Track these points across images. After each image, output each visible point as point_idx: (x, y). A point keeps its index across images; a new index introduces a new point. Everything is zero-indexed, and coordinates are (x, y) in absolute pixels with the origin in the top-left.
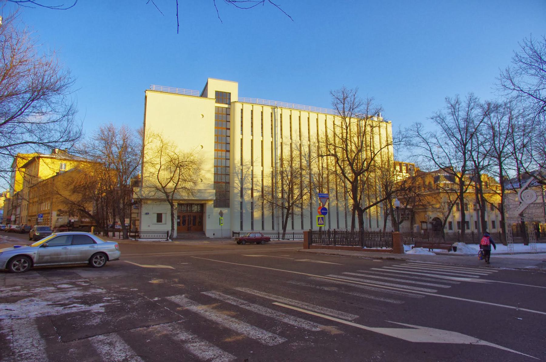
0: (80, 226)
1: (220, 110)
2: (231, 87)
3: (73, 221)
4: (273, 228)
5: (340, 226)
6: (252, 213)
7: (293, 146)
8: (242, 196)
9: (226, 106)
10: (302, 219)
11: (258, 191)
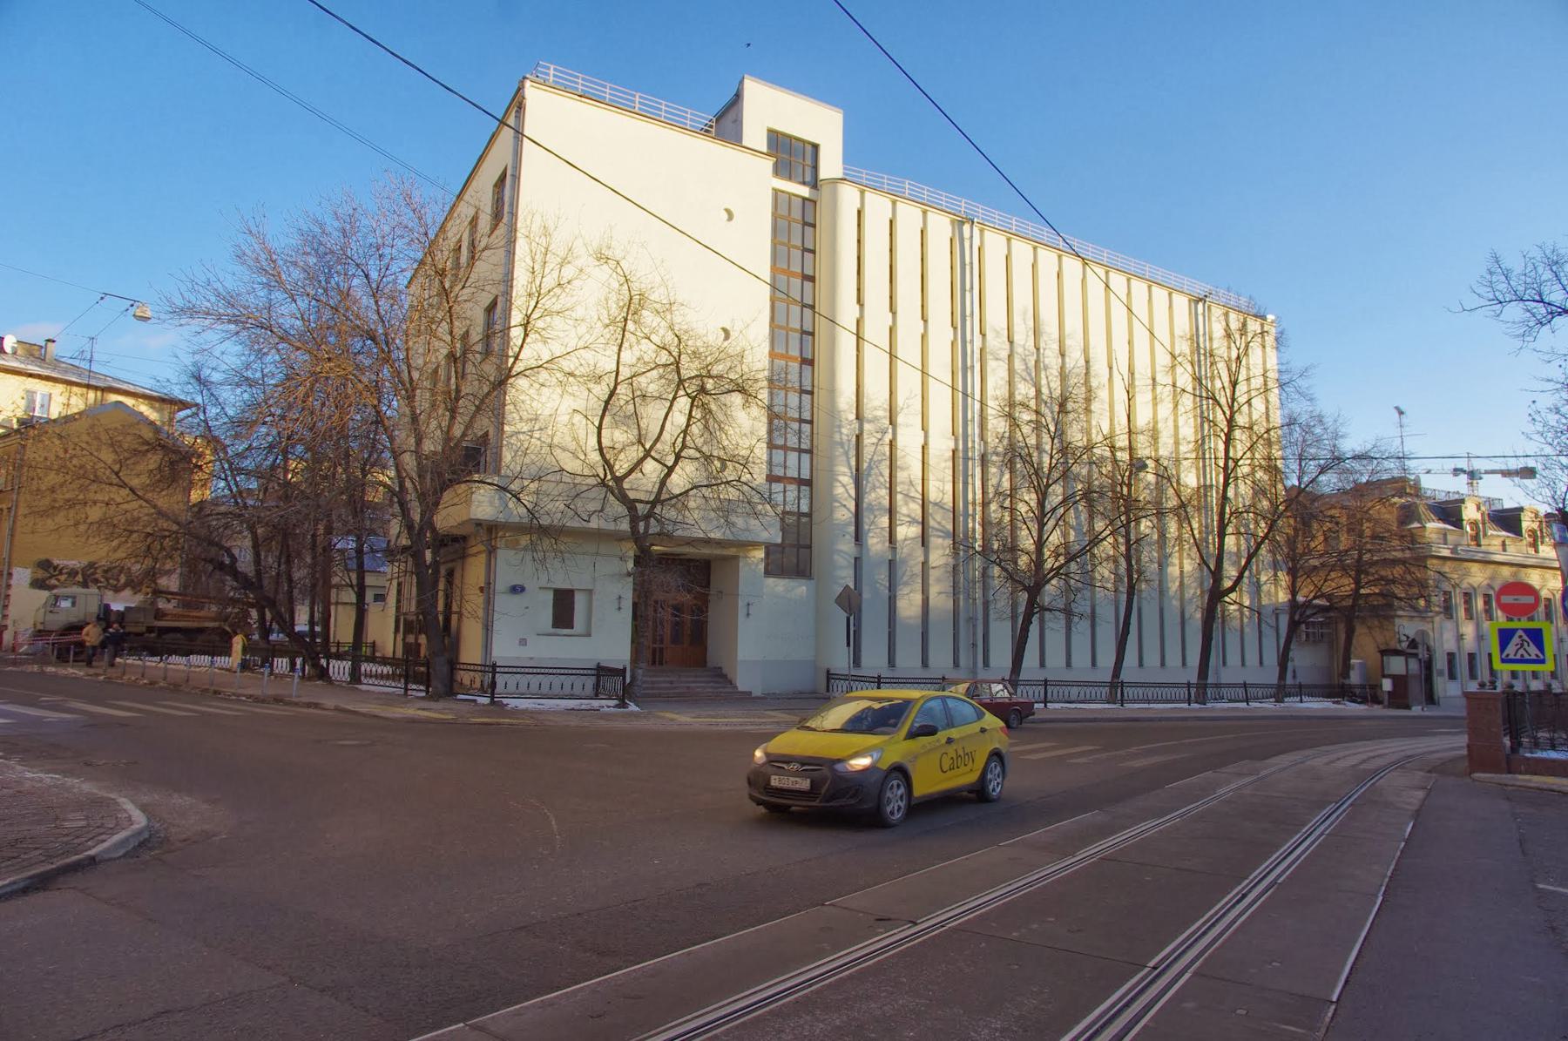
0: (150, 630)
1: (783, 198)
2: (820, 124)
3: (117, 606)
4: (956, 664)
5: (899, 661)
6: (892, 600)
7: (1018, 365)
8: (858, 537)
9: (805, 191)
10: (1093, 626)
11: (912, 521)
